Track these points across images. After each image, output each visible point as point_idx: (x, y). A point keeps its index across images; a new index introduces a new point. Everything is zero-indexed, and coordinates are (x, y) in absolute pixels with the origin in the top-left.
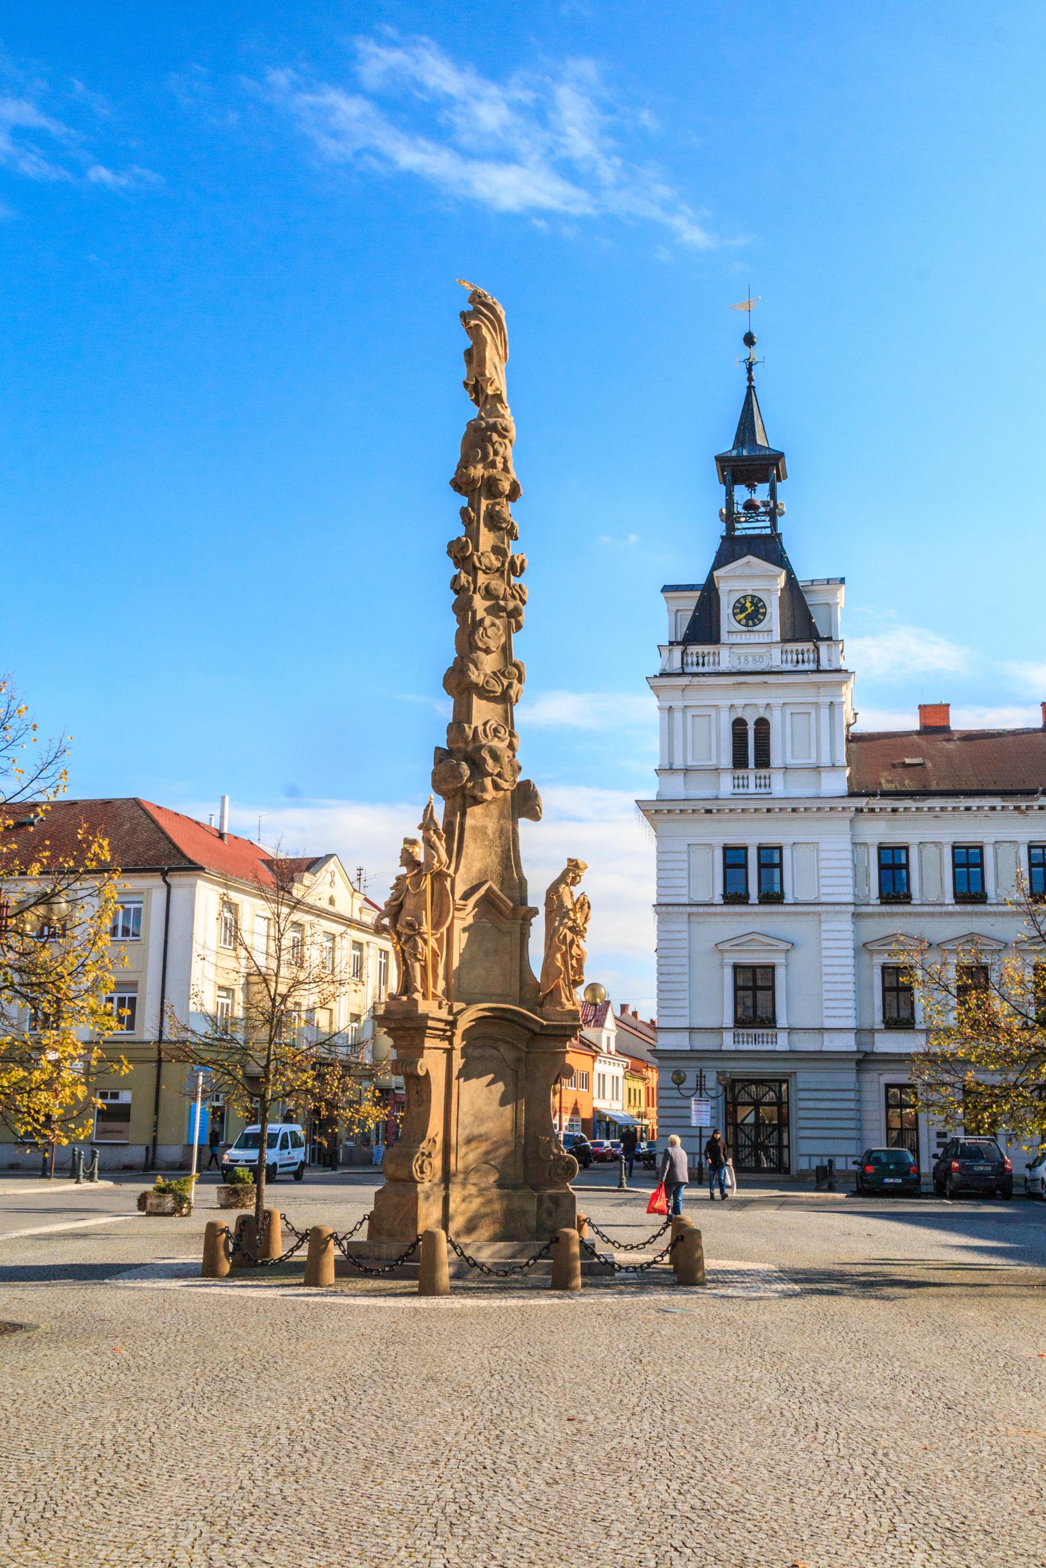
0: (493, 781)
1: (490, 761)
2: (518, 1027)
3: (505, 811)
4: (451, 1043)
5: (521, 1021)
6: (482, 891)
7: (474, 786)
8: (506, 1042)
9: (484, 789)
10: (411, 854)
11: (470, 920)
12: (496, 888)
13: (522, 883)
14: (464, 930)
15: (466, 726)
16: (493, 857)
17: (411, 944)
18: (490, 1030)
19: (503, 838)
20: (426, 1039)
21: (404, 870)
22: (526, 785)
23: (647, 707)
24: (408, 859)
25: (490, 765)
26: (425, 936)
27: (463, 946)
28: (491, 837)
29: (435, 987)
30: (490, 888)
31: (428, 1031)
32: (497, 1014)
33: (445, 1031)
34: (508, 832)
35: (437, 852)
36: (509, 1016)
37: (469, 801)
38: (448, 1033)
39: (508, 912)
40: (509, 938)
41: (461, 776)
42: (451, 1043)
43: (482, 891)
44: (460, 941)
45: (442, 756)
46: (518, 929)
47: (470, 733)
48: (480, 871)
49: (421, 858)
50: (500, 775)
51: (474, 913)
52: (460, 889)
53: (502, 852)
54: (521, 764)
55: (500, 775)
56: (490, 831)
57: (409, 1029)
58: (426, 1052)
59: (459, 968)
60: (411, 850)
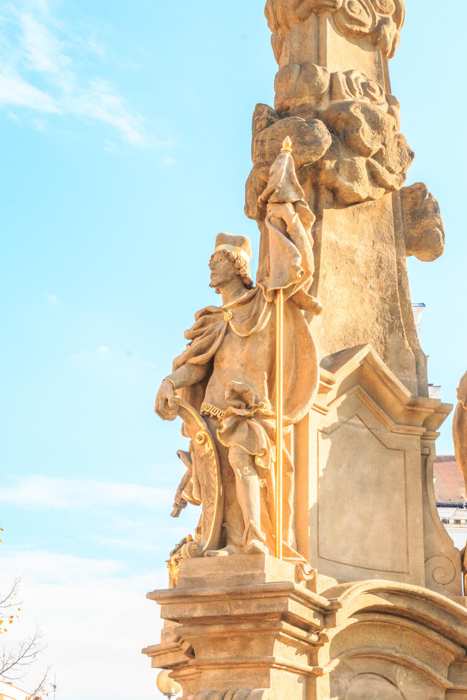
0: (369, 165)
1: (366, 126)
2: (434, 636)
3: (384, 230)
4: (313, 661)
5: (445, 622)
6: (354, 363)
7: (337, 169)
8: (409, 666)
9: (354, 176)
10: (234, 262)
11: (332, 418)
12: (378, 359)
13: (419, 363)
14: (325, 433)
15: (319, 69)
16: (367, 307)
17: (241, 434)
18: (382, 641)
19: (383, 275)
20: (277, 644)
21: (216, 300)
22: (419, 191)
23: (330, 354)
24: (229, 276)
25: (366, 135)
26: (271, 423)
27: (323, 464)
28: (363, 270)
29: (285, 539)
30: (367, 359)
31: (286, 626)
32: (401, 604)
33: (307, 628)
34: (390, 267)
35: (301, 248)
36: (420, 609)
37: (326, 196)
38: (314, 638)
39: (399, 409)
40: (400, 461)
41: (317, 142)
42: (313, 661)
43: (354, 363)
44: (319, 453)
45: (268, 121)
46: (416, 443)
47: (324, 79)
48: (345, 327)
49: (251, 273)
50: (379, 156)
51: (338, 403)
52: (321, 353)
53: (383, 300)
54: (413, 149)
55: (379, 156)
56: (360, 258)
57: (240, 619)
58: (273, 672)
59: (318, 507)
60: (234, 254)
